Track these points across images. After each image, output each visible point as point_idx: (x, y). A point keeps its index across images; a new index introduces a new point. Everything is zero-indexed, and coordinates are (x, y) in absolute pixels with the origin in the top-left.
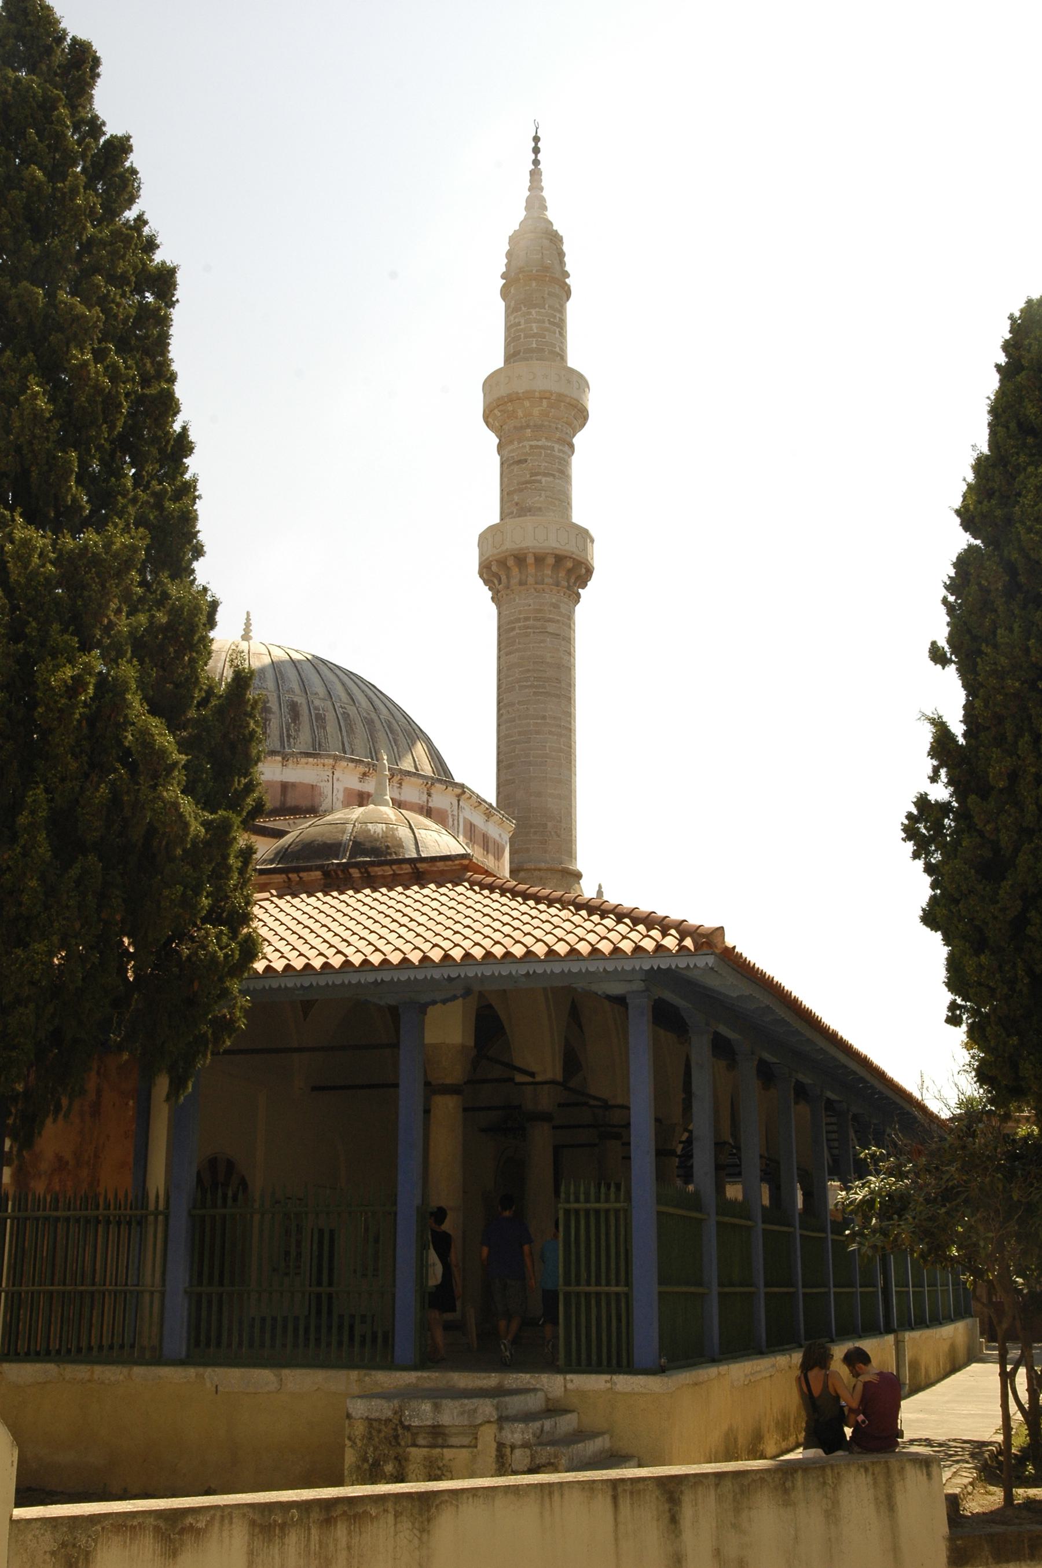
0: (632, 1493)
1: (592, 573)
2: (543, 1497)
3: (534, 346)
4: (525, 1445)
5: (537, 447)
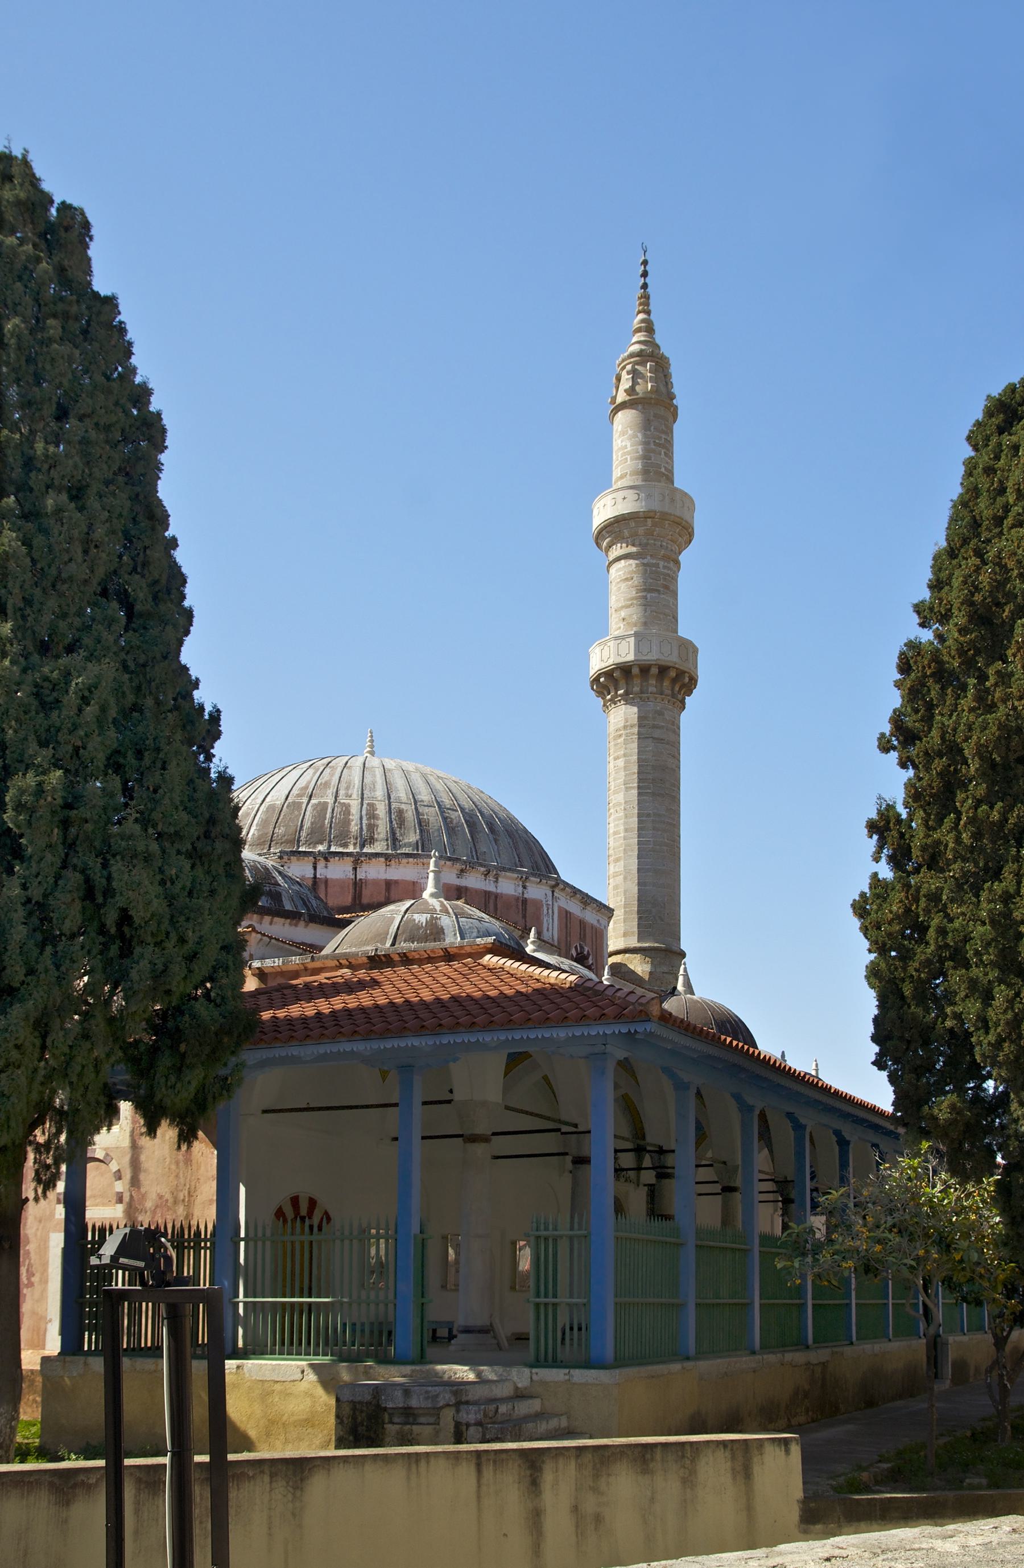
0: (495, 1462)
1: (696, 681)
2: (410, 1464)
4: (479, 1424)
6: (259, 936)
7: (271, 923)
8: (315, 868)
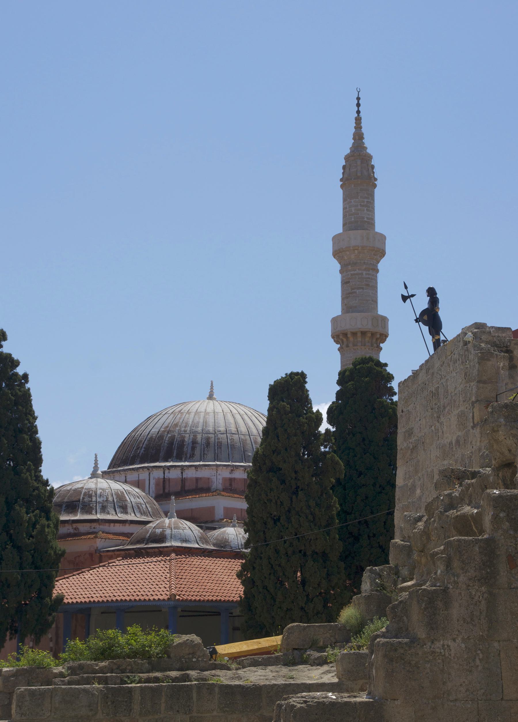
3: (353, 220)
5: (354, 274)
6: (100, 539)
7: (114, 526)
8: (164, 473)
